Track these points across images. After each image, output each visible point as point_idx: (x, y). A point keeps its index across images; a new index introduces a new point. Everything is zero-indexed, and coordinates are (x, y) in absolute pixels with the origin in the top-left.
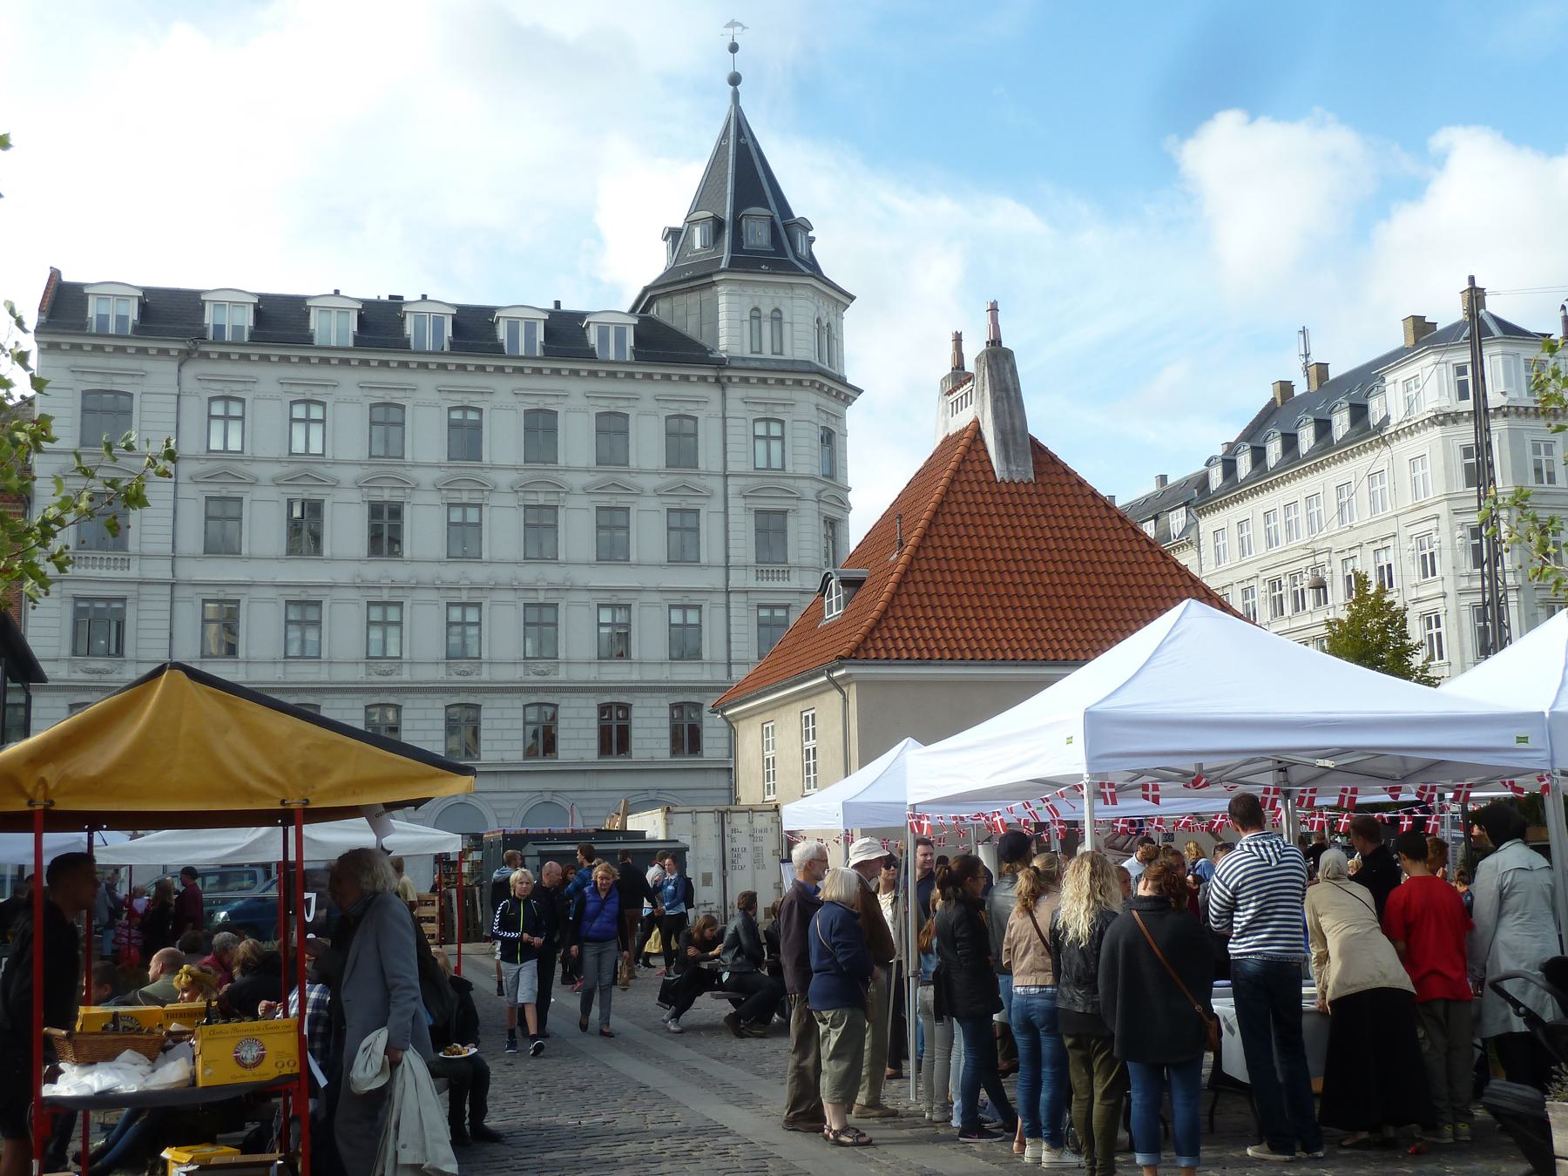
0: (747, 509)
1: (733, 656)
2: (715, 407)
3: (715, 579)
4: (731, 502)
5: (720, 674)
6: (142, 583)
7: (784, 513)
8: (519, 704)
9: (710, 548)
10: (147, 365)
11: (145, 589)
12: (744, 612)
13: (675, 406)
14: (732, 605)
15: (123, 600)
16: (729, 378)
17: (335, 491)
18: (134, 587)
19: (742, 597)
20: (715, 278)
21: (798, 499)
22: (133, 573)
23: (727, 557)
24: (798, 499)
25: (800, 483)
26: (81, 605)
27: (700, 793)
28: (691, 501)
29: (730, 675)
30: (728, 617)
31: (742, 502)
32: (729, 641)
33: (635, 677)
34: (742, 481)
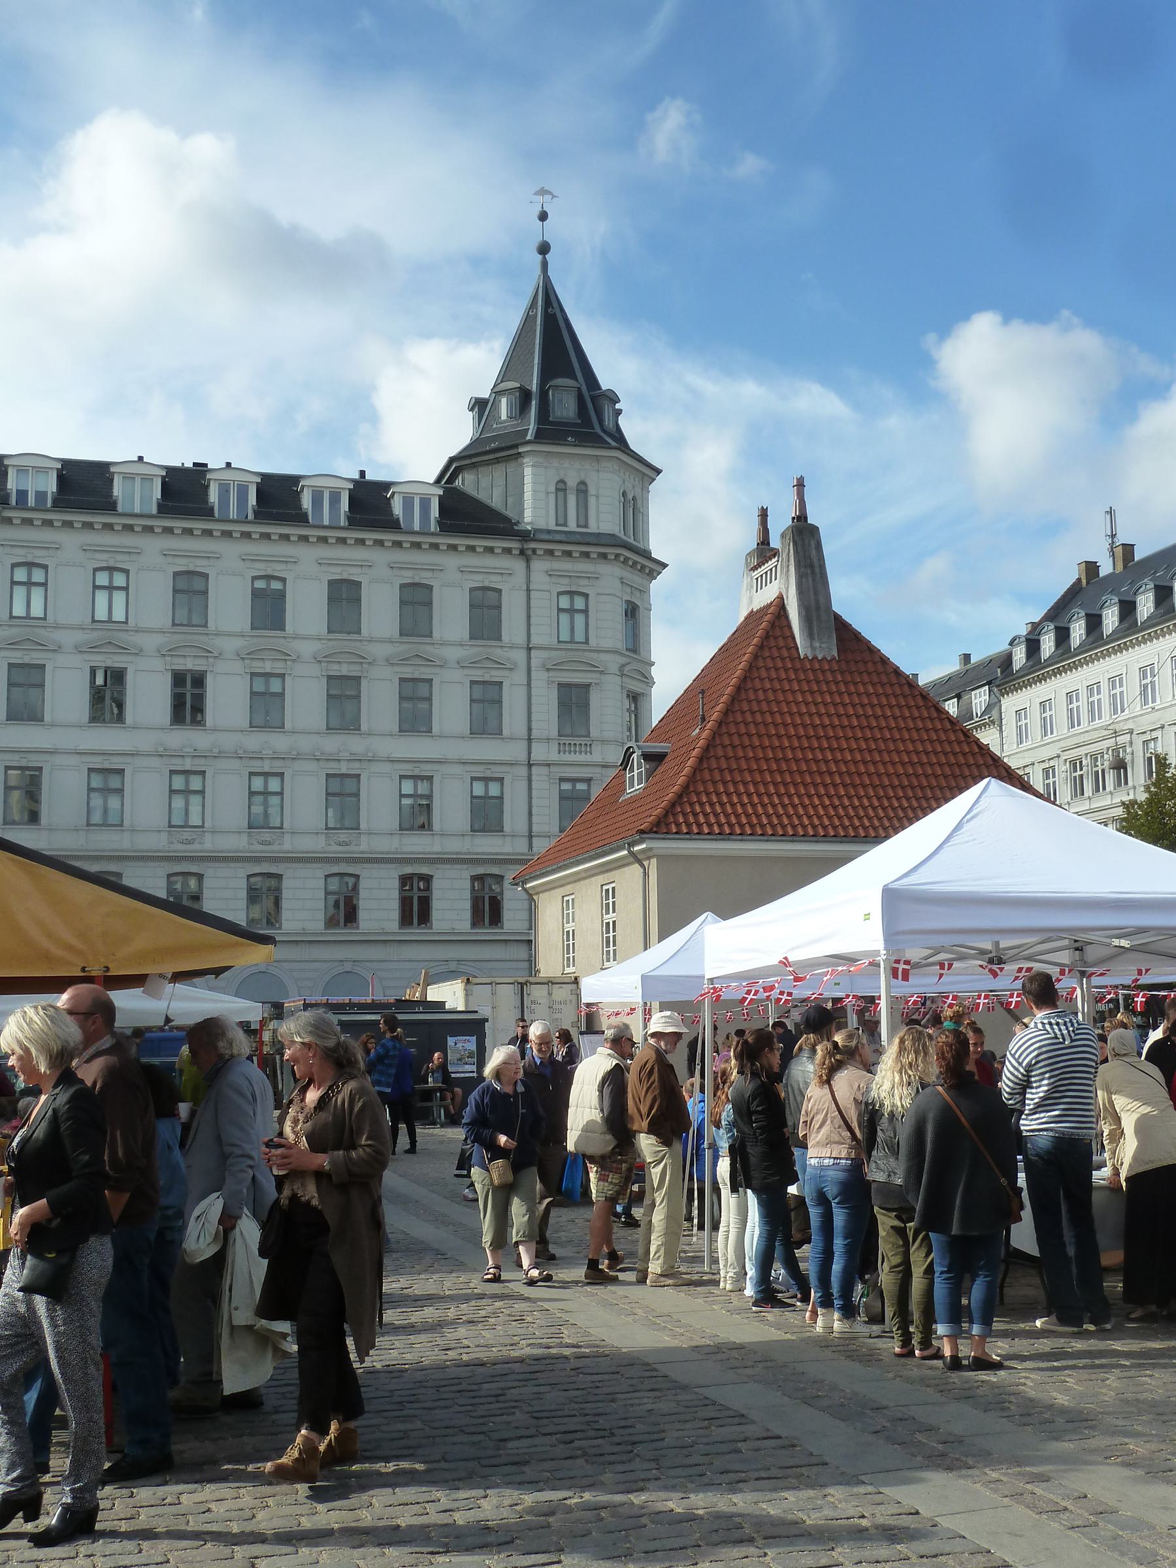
1: (534, 829)
3: (517, 752)
4: (533, 674)
5: (521, 846)
14: (534, 778)
16: (534, 551)
18: (598, 770)
19: (545, 770)
21: (602, 672)
24: (602, 672)
25: (603, 657)
31: (545, 675)
33: (437, 848)
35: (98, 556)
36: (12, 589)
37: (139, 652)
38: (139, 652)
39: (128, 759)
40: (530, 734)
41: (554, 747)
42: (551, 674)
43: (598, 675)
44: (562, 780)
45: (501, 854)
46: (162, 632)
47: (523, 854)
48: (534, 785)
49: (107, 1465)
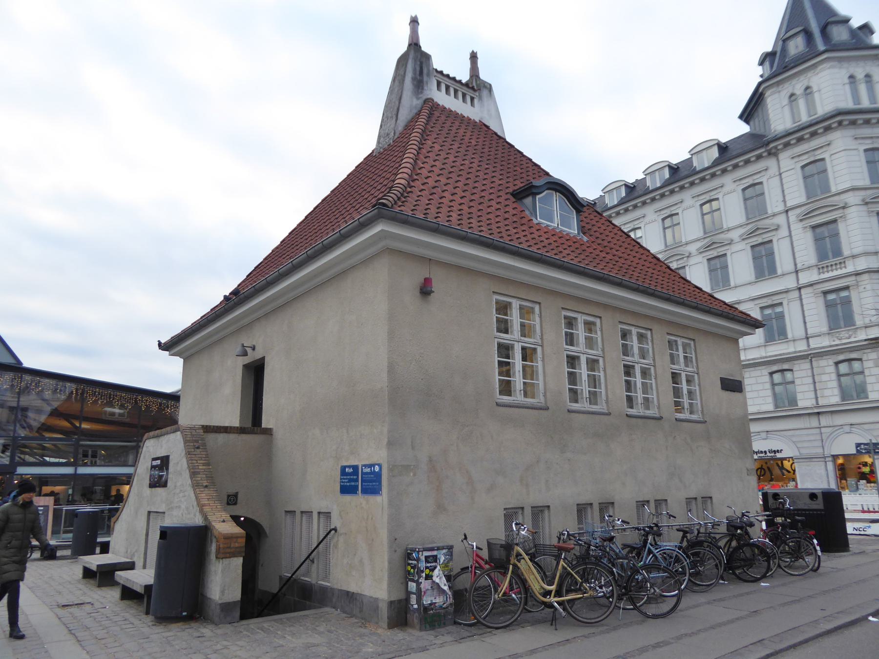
0: (870, 212)
1: (809, 332)
2: (773, 170)
3: (789, 283)
4: (792, 228)
5: (802, 346)
6: (858, 274)
7: (834, 221)
8: (831, 362)
9: (783, 262)
10: (638, 213)
11: (859, 278)
12: (813, 300)
13: (665, 211)
14: (803, 297)
15: (847, 288)
16: (776, 147)
17: (732, 246)
18: (853, 278)
19: (810, 290)
20: (761, 90)
21: (844, 208)
22: (850, 268)
23: (796, 265)
24: (844, 208)
25: (843, 197)
26: (831, 297)
27: (798, 432)
28: (765, 236)
29: (809, 345)
30: (802, 305)
31: (801, 225)
32: (805, 323)
33: (792, 350)
34: (798, 211)
35: (663, 212)
36: (664, 232)
37: (731, 242)
38: (731, 242)
39: (784, 295)
40: (796, 267)
41: (815, 271)
42: (804, 223)
43: (841, 211)
44: (825, 293)
45: (784, 354)
46: (698, 240)
47: (805, 351)
48: (804, 302)
49: (184, 614)
